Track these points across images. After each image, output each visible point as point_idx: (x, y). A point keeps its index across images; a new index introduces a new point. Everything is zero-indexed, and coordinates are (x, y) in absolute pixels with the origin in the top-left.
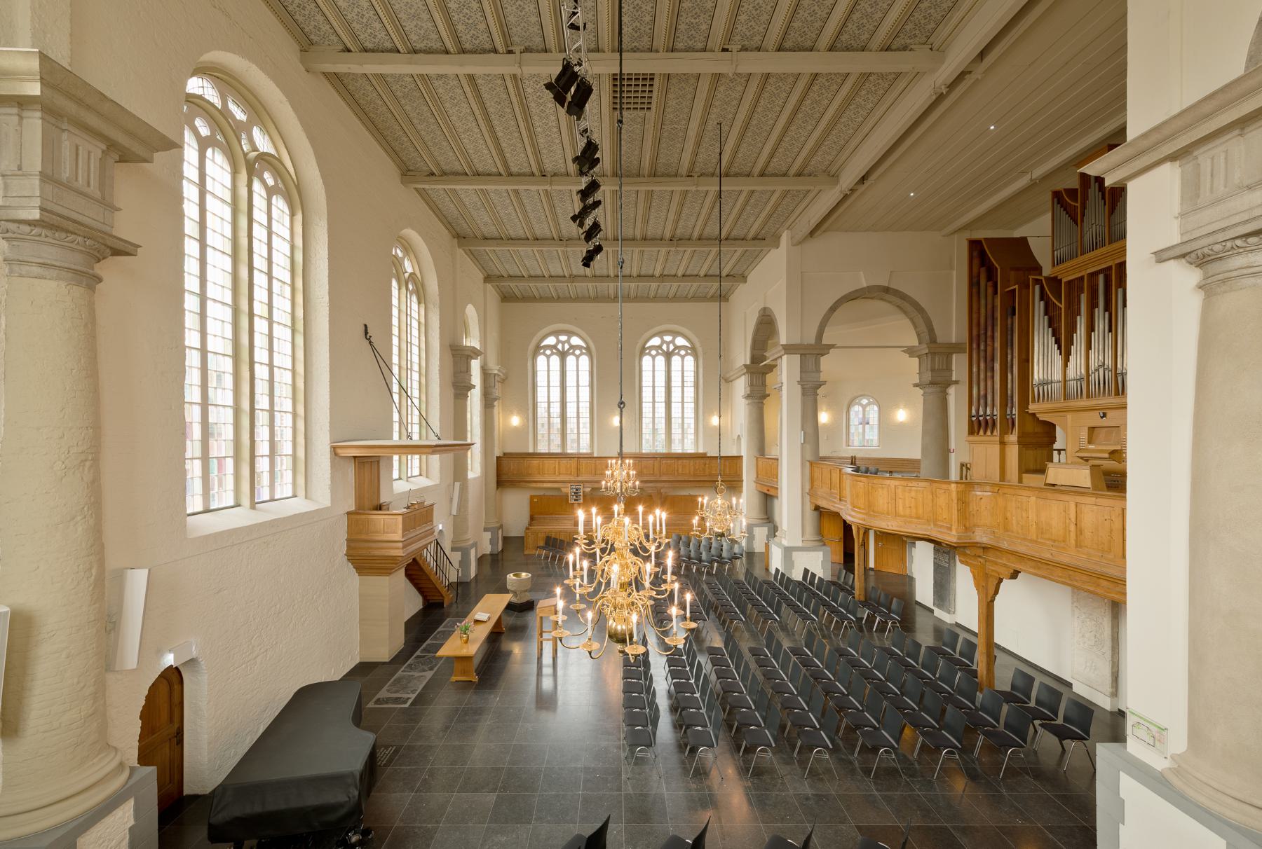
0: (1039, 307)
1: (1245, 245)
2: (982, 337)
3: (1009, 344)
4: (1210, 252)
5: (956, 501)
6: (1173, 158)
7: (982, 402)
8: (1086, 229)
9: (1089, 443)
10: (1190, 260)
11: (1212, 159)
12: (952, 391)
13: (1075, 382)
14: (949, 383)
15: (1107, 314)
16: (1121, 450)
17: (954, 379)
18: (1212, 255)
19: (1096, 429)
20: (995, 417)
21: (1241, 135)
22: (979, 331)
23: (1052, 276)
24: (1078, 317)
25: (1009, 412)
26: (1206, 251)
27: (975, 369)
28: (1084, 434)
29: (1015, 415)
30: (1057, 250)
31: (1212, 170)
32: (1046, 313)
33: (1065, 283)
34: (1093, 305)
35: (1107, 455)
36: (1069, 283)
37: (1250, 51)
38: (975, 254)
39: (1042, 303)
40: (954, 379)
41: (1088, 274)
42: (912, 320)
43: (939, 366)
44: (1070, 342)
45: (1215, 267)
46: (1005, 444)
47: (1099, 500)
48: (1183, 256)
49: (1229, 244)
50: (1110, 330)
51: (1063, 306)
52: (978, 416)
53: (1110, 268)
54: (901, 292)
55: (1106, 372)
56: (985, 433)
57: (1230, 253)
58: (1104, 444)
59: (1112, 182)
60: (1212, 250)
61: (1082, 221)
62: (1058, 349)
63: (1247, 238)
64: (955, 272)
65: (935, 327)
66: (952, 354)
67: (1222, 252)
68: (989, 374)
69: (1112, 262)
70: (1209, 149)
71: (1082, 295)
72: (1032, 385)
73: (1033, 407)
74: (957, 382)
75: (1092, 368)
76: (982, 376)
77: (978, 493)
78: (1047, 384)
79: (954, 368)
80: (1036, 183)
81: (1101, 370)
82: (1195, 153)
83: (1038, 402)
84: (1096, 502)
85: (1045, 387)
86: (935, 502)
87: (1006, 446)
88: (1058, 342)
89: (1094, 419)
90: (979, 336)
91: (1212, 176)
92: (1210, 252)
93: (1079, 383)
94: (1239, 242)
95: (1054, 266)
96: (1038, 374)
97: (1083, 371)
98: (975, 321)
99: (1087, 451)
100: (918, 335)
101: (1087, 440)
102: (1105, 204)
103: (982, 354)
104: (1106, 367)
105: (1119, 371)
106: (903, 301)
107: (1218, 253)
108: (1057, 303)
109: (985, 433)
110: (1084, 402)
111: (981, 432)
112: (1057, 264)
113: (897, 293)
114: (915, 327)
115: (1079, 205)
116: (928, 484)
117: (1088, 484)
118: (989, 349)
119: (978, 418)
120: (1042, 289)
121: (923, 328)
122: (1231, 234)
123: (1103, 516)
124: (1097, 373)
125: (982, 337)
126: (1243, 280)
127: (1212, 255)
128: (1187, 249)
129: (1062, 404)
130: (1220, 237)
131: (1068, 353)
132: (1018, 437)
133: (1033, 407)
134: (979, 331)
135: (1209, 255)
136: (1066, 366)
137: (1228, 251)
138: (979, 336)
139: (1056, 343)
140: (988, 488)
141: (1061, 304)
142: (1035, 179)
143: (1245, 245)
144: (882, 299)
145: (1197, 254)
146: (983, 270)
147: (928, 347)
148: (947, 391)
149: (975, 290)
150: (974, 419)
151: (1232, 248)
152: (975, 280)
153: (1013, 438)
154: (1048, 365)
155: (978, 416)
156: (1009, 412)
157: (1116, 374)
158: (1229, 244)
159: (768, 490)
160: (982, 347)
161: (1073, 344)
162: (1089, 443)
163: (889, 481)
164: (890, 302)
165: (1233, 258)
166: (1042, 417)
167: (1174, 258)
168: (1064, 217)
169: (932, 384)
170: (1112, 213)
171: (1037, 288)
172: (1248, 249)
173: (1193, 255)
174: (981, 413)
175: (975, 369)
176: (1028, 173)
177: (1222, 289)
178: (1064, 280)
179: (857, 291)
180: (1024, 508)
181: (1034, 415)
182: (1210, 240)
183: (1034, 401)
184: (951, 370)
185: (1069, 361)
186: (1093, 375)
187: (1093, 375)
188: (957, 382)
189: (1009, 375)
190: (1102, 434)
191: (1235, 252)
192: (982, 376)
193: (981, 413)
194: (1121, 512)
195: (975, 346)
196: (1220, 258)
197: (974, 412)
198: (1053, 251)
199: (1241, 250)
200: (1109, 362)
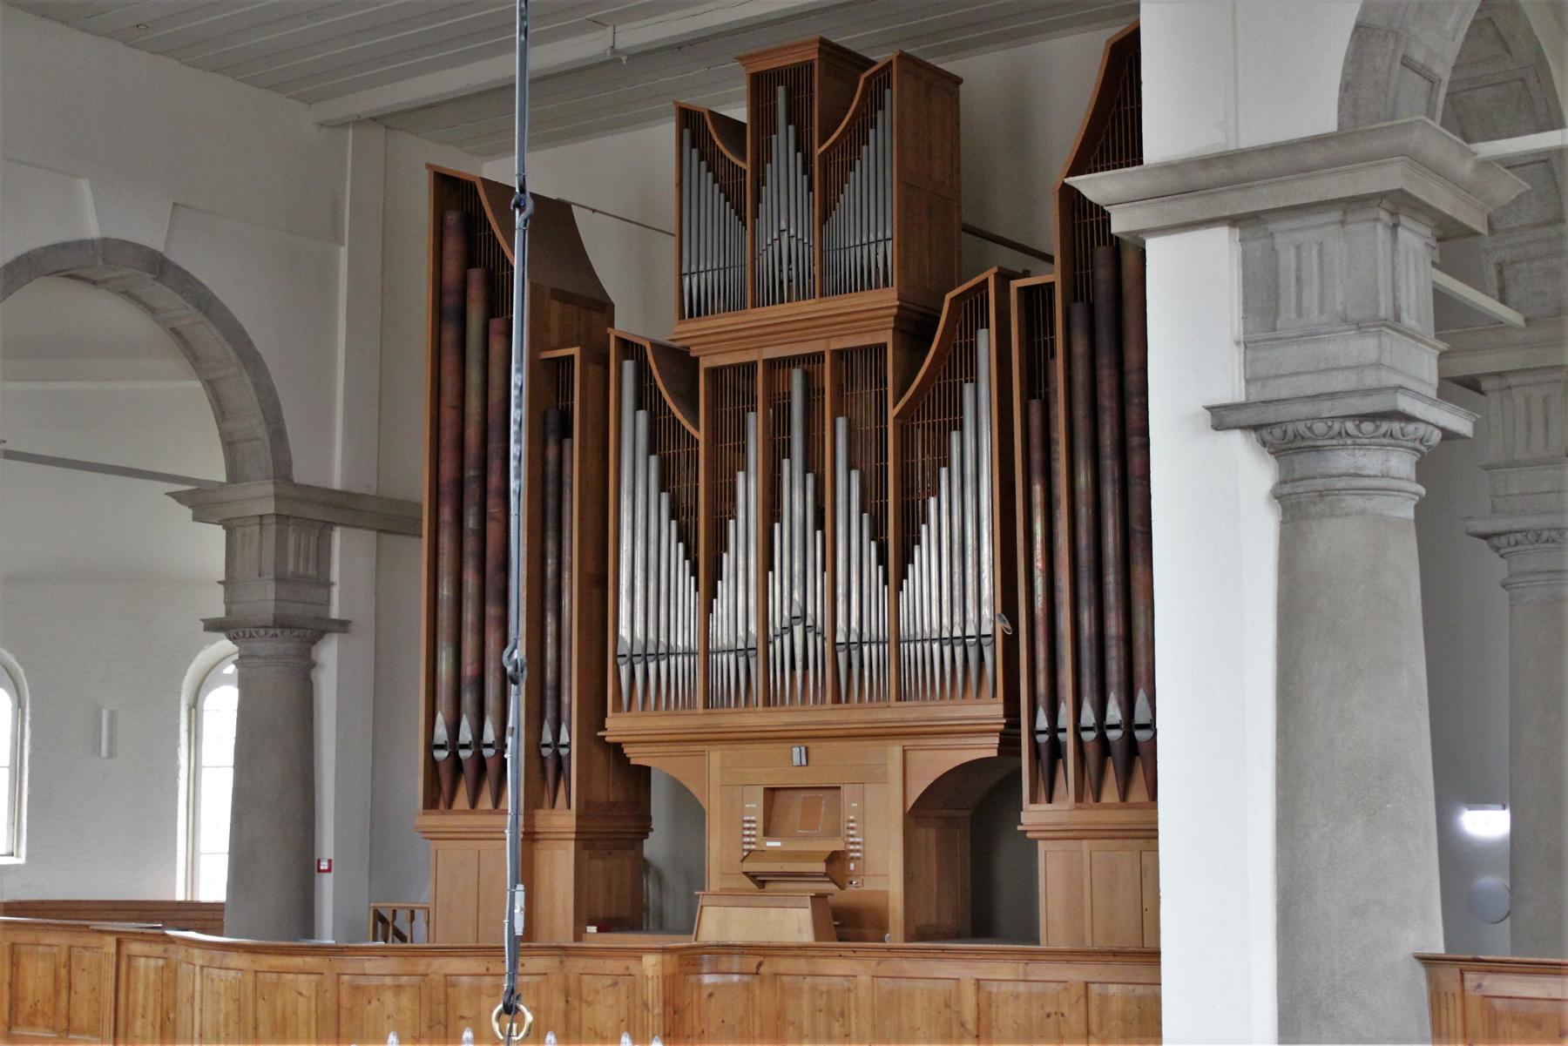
0: (633, 427)
1: (1356, 433)
2: (472, 490)
3: (551, 524)
4: (1308, 433)
5: (658, 1010)
6: (1233, 221)
7: (468, 699)
8: (765, 240)
9: (767, 833)
10: (1268, 437)
11: (1298, 248)
12: (328, 652)
13: (732, 657)
14: (321, 628)
15: (810, 478)
16: (844, 852)
17: (335, 613)
18: (1309, 439)
19: (777, 792)
20: (563, 751)
21: (1342, 223)
22: (461, 468)
23: (677, 344)
24: (741, 476)
25: (548, 737)
26: (1301, 428)
27: (445, 591)
28: (754, 807)
29: (568, 745)
30: (690, 274)
31: (1298, 270)
32: (652, 449)
33: (707, 370)
34: (777, 451)
35: (820, 867)
36: (714, 372)
37: (1344, 75)
38: (452, 218)
39: (642, 415)
40: (335, 613)
41: (765, 361)
42: (213, 389)
43: (297, 565)
44: (719, 543)
45: (1305, 463)
46: (534, 840)
47: (1032, 967)
48: (1256, 428)
49: (1337, 426)
50: (819, 524)
51: (701, 436)
52: (454, 743)
53: (819, 357)
54: (200, 284)
55: (810, 636)
56: (474, 802)
57: (1335, 442)
58: (804, 837)
59: (1120, 231)
60: (1310, 429)
61: (756, 215)
62: (686, 557)
63: (1361, 422)
64: (343, 252)
65: (289, 429)
66: (330, 525)
67: (1323, 436)
68: (492, 611)
69: (823, 342)
70: (1291, 230)
71: (751, 415)
72: (616, 656)
73: (617, 726)
74: (343, 626)
75: (776, 622)
76: (469, 616)
77: (708, 979)
78: (690, 654)
79: (335, 575)
80: (620, 60)
81: (798, 630)
82: (1272, 227)
83: (847, 701)
84: (1025, 973)
85: (652, 666)
86: (575, 1018)
87: (539, 845)
88: (686, 536)
89: (789, 766)
90: (460, 483)
91: (1298, 279)
92: (1308, 433)
93: (742, 661)
94: (1350, 426)
95: (682, 317)
96: (628, 626)
97: (752, 628)
98: (448, 436)
99: (761, 854)
100: (230, 445)
101: (760, 826)
102: (811, 188)
103: (470, 544)
104: (809, 622)
105: (841, 638)
106: (200, 317)
107: (1317, 438)
108: (684, 422)
109: (474, 802)
110: (757, 718)
111: (462, 799)
112: (691, 315)
113: (185, 283)
114: (221, 415)
115: (747, 167)
116: (556, 961)
117: (807, 937)
118: (493, 529)
119: (454, 755)
120: (642, 372)
121: (253, 425)
122: (1342, 407)
123: (1043, 1007)
124: (787, 638)
125: (472, 490)
126: (1348, 498)
127: (1309, 439)
128: (1270, 415)
129: (697, 719)
130: (1327, 409)
131: (715, 574)
132: (579, 817)
133: (617, 726)
134: (461, 468)
135: (1303, 438)
136: (709, 609)
137: (1333, 438)
138: (460, 483)
139: (679, 540)
140: (735, 962)
141: (697, 428)
142: (622, 52)
143: (1356, 433)
144: (128, 294)
145: (1285, 432)
146: (476, 275)
147: (277, 496)
148: (313, 656)
149: (449, 336)
150: (441, 755)
151: (1340, 433)
152: (450, 301)
153: (562, 819)
154: (658, 599)
155: (454, 743)
156: (548, 737)
157: (835, 644)
158: (1337, 426)
159: (1146, 910)
160: (471, 522)
161: (726, 549)
162: (767, 833)
163: (424, 961)
164: (151, 310)
165: (1336, 453)
166: (636, 756)
167: (1243, 428)
168: (710, 192)
169: (282, 627)
170: (826, 219)
171: (629, 365)
172: (1358, 441)
173: (1278, 432)
174: (466, 735)
175: (445, 591)
176: (605, 26)
177: (1318, 508)
178: (705, 363)
179: (64, 246)
180: (837, 1010)
181: (617, 748)
182: (1306, 409)
183: (618, 707)
184: (328, 584)
185: (716, 596)
186: (778, 642)
187: (778, 642)
188: (343, 626)
189: (550, 619)
190: (794, 807)
191: (1341, 442)
192: (469, 616)
193: (466, 735)
194: (1082, 992)
195: (446, 514)
196: (1317, 449)
197: (441, 734)
198: (681, 276)
199: (1349, 441)
200: (816, 609)
